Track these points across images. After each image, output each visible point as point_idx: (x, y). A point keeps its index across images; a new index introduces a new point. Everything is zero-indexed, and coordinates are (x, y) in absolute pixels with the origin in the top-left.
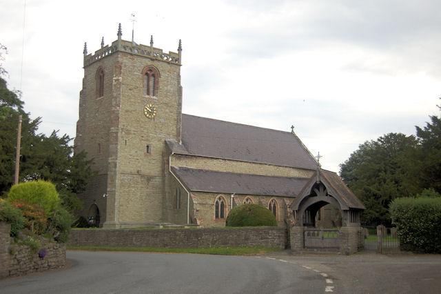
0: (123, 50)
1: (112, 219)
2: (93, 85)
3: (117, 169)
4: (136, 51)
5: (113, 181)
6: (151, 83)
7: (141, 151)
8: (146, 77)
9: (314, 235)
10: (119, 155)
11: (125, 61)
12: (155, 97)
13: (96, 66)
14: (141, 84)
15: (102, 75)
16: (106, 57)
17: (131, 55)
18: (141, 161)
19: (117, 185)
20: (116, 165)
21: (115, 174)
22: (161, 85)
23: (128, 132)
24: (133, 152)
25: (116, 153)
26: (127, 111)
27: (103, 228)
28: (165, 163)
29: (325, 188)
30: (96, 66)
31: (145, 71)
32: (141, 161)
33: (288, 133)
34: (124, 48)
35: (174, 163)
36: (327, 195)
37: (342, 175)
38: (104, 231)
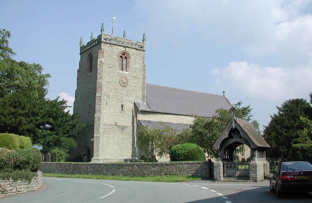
0: (104, 41)
1: (98, 156)
2: (87, 65)
3: (101, 122)
4: (114, 42)
5: (98, 130)
6: (124, 63)
7: (117, 109)
8: (121, 58)
9: (231, 167)
10: (102, 112)
11: (106, 48)
12: (127, 72)
13: (88, 53)
14: (117, 63)
15: (91, 58)
16: (94, 46)
17: (111, 44)
18: (117, 116)
19: (101, 132)
20: (100, 118)
21: (99, 125)
22: (131, 63)
23: (108, 97)
24: (112, 110)
25: (100, 111)
26: (108, 82)
27: (91, 162)
28: (134, 117)
29: (239, 132)
30: (88, 53)
31: (120, 55)
32: (117, 116)
33: (221, 96)
34: (105, 39)
35: (141, 117)
36: (241, 137)
37: (268, 131)
38: (92, 164)
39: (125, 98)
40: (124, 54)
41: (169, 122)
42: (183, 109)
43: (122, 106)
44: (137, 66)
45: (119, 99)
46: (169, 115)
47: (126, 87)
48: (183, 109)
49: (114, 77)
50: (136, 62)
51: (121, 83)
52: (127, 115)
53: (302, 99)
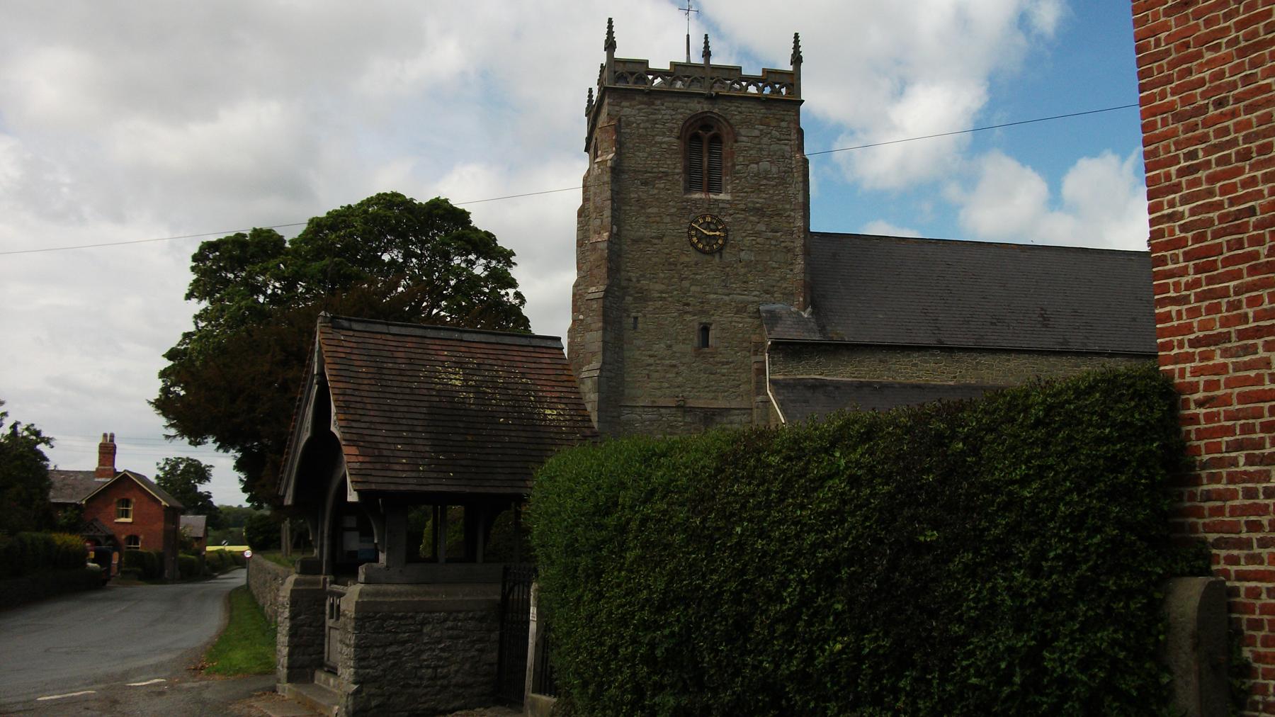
39: (713, 296)
40: (706, 127)
41: (914, 381)
42: (992, 324)
43: (705, 329)
44: (765, 165)
45: (688, 305)
46: (916, 355)
47: (717, 256)
48: (992, 324)
49: (668, 219)
50: (761, 149)
51: (695, 240)
52: (723, 363)
53: (257, 233)
